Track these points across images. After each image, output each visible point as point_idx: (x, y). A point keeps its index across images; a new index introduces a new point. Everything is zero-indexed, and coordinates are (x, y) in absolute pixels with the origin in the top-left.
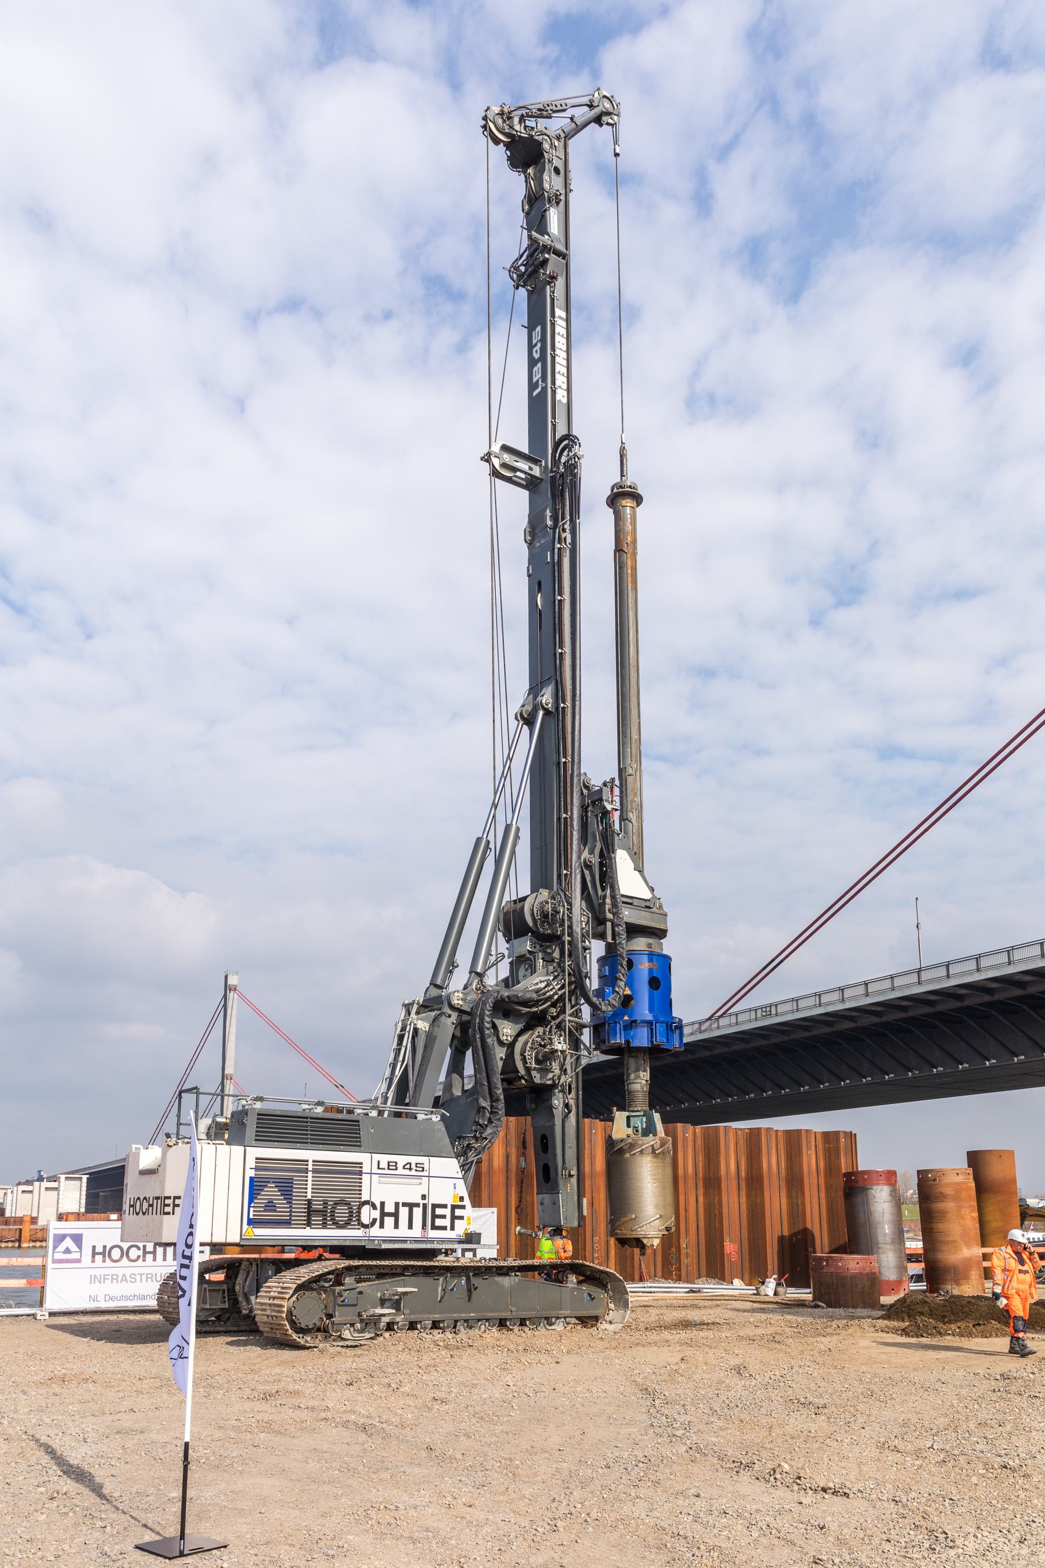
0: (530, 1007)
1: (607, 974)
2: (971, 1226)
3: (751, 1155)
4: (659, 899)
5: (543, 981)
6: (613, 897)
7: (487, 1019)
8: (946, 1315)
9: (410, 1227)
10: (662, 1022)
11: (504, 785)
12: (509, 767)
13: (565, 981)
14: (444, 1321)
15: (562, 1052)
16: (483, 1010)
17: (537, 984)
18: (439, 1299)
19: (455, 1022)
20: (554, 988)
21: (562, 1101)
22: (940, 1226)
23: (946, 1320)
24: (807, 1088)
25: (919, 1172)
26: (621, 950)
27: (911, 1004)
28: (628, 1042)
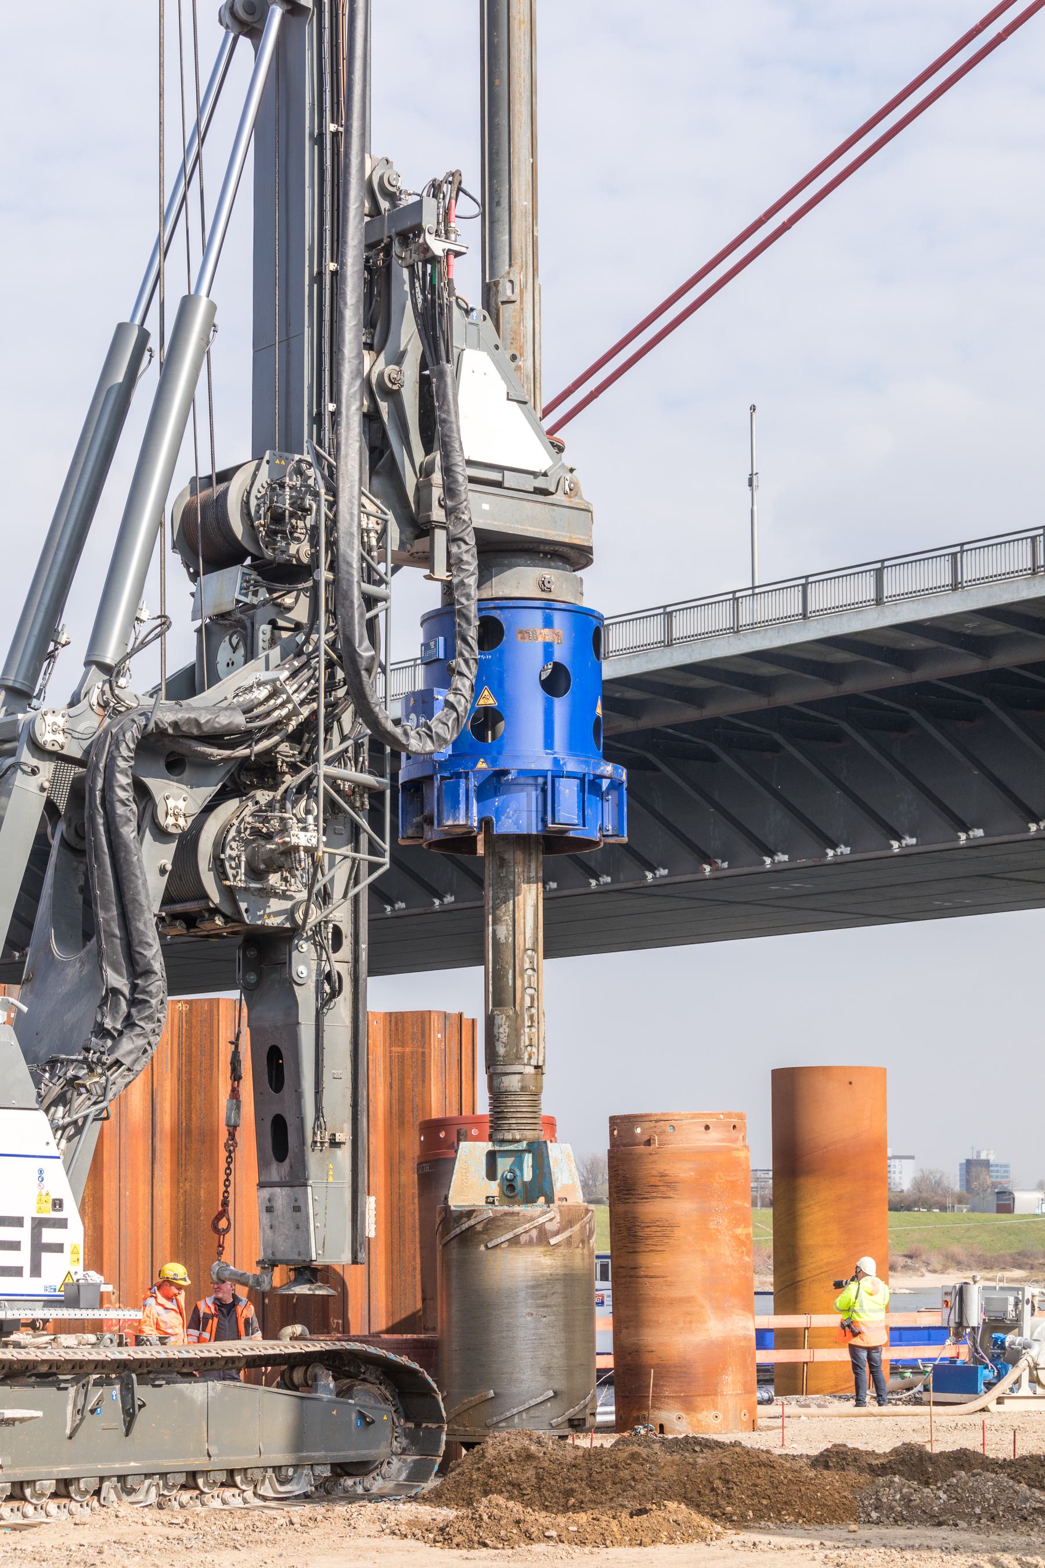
0: (232, 746)
1: (442, 656)
2: (730, 1261)
3: (189, 1072)
4: (572, 470)
5: (264, 683)
6: (448, 471)
7: (123, 780)
8: (573, 1490)
9: (15, 1246)
10: (571, 776)
11: (184, 198)
12: (198, 156)
13: (318, 681)
14: (78, 1479)
15: (310, 851)
16: (111, 760)
17: (250, 689)
18: (68, 1432)
19: (47, 785)
20: (289, 700)
21: (314, 965)
22: (653, 1262)
23: (572, 1501)
24: (449, 899)
25: (614, 1121)
26: (463, 600)
27: (784, 671)
28: (486, 824)
